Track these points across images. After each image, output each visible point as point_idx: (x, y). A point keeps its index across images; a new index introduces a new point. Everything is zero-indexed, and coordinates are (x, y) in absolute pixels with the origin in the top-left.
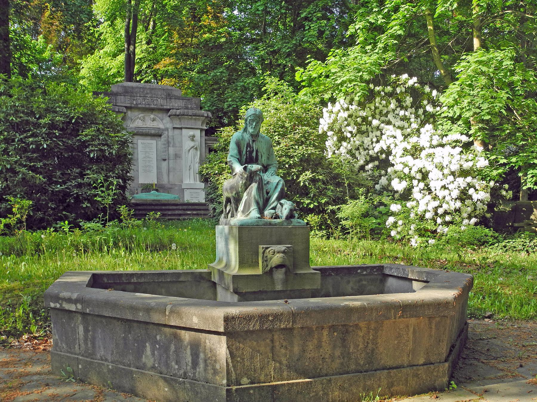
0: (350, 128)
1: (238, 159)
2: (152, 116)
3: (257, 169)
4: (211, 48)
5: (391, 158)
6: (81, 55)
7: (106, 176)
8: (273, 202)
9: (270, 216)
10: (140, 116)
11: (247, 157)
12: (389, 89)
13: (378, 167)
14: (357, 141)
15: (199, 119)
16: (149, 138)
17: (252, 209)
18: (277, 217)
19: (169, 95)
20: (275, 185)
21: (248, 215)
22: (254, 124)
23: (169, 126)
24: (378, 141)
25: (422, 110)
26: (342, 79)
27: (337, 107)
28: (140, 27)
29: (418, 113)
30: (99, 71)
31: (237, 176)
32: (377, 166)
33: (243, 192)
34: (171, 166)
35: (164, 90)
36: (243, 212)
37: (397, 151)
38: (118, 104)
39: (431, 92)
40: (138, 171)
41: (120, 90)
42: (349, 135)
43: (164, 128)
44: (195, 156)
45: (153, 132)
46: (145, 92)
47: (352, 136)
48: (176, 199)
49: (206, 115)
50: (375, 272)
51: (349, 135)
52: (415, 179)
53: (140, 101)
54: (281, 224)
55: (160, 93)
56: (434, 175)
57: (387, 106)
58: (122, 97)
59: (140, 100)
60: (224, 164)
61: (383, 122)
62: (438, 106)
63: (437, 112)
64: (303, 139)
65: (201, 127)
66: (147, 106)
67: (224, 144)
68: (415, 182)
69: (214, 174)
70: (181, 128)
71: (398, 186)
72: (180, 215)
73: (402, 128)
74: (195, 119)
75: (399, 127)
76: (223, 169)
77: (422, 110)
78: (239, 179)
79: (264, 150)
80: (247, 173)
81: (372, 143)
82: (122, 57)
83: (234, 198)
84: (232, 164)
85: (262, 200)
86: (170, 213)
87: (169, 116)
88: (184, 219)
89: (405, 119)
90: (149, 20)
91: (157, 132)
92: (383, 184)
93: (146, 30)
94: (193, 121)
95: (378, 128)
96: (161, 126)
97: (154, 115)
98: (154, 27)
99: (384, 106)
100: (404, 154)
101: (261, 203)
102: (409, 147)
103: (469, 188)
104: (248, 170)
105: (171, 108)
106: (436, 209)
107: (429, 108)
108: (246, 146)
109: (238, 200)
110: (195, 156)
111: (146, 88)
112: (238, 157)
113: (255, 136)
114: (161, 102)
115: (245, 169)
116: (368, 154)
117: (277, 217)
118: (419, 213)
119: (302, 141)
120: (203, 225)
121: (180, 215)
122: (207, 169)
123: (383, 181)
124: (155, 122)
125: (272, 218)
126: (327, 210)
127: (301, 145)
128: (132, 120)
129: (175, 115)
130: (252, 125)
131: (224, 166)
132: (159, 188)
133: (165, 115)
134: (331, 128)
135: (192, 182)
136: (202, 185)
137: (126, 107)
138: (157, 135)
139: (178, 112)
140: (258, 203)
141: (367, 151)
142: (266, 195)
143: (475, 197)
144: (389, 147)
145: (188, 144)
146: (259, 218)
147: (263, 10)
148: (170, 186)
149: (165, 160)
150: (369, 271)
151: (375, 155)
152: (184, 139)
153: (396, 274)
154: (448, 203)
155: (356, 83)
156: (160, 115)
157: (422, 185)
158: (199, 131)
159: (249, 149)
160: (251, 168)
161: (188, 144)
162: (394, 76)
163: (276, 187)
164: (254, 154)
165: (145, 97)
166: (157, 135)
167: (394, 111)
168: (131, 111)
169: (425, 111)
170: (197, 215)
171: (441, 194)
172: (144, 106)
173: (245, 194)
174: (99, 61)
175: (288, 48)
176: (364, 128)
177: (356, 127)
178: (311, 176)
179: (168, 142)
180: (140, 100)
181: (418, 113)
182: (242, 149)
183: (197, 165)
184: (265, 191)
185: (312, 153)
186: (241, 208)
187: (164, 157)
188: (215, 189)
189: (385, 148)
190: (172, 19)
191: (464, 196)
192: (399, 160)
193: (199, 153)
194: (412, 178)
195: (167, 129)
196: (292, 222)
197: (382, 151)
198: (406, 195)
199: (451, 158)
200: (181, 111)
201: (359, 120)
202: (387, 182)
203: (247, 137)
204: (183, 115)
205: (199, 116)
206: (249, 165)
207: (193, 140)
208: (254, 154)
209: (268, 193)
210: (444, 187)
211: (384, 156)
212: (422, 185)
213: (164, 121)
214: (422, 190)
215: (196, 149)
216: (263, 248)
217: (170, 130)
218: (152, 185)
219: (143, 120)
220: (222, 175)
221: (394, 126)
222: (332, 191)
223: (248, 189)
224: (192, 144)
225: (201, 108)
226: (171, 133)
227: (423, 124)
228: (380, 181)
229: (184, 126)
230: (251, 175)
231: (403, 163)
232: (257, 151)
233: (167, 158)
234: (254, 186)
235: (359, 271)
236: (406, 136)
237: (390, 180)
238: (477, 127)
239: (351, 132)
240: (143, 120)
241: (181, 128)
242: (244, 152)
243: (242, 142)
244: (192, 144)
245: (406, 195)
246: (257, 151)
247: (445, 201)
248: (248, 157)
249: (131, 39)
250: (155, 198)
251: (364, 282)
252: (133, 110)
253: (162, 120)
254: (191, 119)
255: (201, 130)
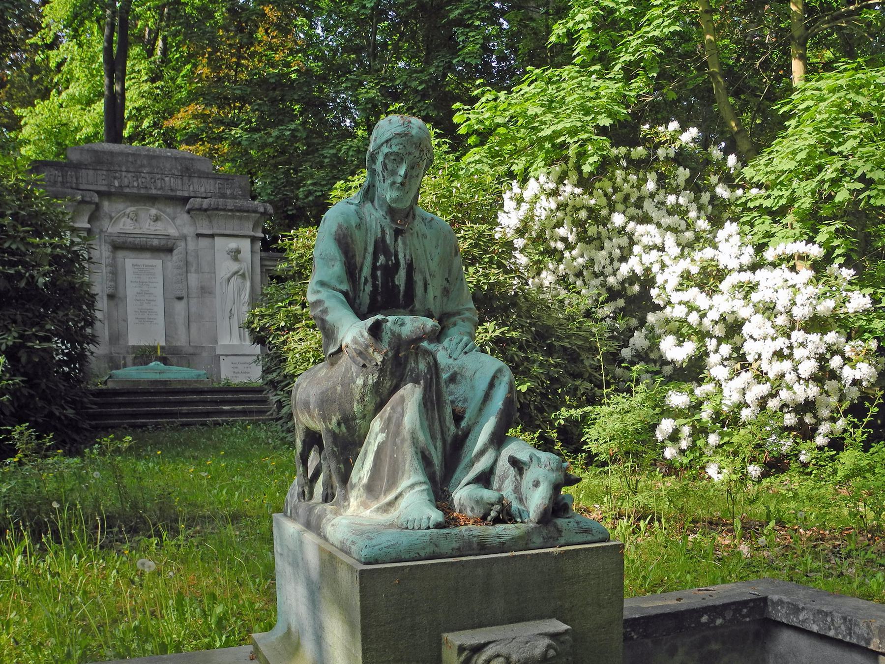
0: (562, 232)
1: (345, 294)
2: (153, 211)
3: (419, 333)
4: (273, 92)
5: (654, 292)
6: (28, 103)
7: (21, 336)
8: (482, 453)
9: (479, 512)
10: (128, 211)
11: (375, 286)
12: (639, 152)
13: (622, 312)
14: (577, 257)
15: (247, 218)
16: (148, 255)
17: (404, 483)
18: (506, 515)
19: (187, 169)
20: (482, 386)
21: (391, 504)
22: (402, 172)
23: (189, 230)
24: (624, 259)
25: (708, 194)
26: (553, 128)
27: (532, 187)
28: (135, 50)
29: (701, 202)
30: (59, 134)
31: (345, 360)
32: (622, 309)
33: (368, 417)
34: (193, 309)
35: (176, 159)
36: (371, 489)
37: (669, 278)
38: (81, 187)
39: (725, 159)
40: (126, 321)
41: (86, 158)
42: (560, 246)
43: (177, 234)
44: (240, 291)
45: (155, 242)
46: (139, 162)
47: (566, 248)
48: (201, 378)
49: (262, 210)
50: (744, 616)
51: (560, 246)
52: (711, 337)
53: (127, 180)
54: (523, 541)
55: (168, 166)
56: (755, 325)
57: (639, 187)
58: (91, 172)
59: (127, 178)
60: (298, 307)
61: (632, 218)
62: (738, 186)
63: (737, 199)
64: (476, 252)
65: (252, 234)
66: (143, 191)
67: (297, 264)
68: (711, 344)
69: (278, 329)
70: (212, 236)
71: (675, 351)
72: (208, 414)
73: (675, 230)
74: (240, 218)
75: (669, 228)
76: (297, 319)
77: (708, 194)
78: (354, 368)
79: (434, 265)
80: (385, 347)
81: (612, 261)
82: (100, 106)
83: (334, 436)
84: (325, 311)
85: (439, 443)
86: (185, 409)
87: (188, 212)
88: (217, 424)
89: (676, 210)
90: (156, 39)
91: (163, 242)
92: (638, 347)
93: (150, 56)
94: (236, 222)
95: (621, 231)
96: (172, 231)
97: (158, 209)
98: (165, 52)
99: (632, 187)
100: (682, 285)
101: (437, 458)
102: (695, 270)
103: (832, 355)
104: (386, 337)
105: (192, 194)
106: (762, 403)
107: (722, 191)
108: (371, 249)
109: (347, 446)
110: (240, 291)
111: (140, 155)
112: (345, 287)
113: (402, 216)
114: (172, 184)
115: (375, 331)
116: (604, 285)
117: (506, 515)
118: (726, 409)
119: (474, 257)
120: (256, 439)
121: (208, 414)
122: (262, 316)
123: (639, 339)
124: (159, 223)
125: (484, 518)
126: (556, 419)
127: (473, 264)
128: (111, 218)
129: (200, 209)
130: (394, 173)
131: (299, 312)
132: (168, 355)
133: (179, 209)
134: (521, 232)
135: (236, 341)
136: (257, 349)
137: (100, 193)
138: (165, 249)
139: (206, 203)
140: (425, 459)
141: (602, 278)
142: (453, 428)
143: (848, 373)
144: (648, 270)
145: (226, 267)
146: (438, 526)
147: (372, 9)
148: (191, 351)
149: (180, 298)
150: (729, 615)
151: (617, 287)
152: (218, 256)
153: (815, 628)
154: (790, 388)
155: (585, 136)
156: (169, 210)
157: (726, 349)
158: (248, 241)
159: (382, 259)
160: (396, 329)
161: (226, 267)
162: (647, 126)
163: (487, 397)
164: (401, 279)
165: (137, 174)
166: (165, 249)
167: (652, 196)
168: (110, 200)
169: (714, 197)
170: (244, 413)
171: (774, 369)
172: (135, 191)
173: (376, 424)
174: (59, 112)
175: (421, 83)
176: (592, 230)
177: (574, 229)
178: (497, 333)
179: (187, 264)
180: (127, 178)
181: (701, 202)
182: (358, 259)
183: (245, 308)
184: (448, 410)
185: (498, 283)
186: (362, 472)
187: (179, 293)
188: (281, 361)
189: (639, 270)
190: (194, 30)
191: (824, 375)
192: (675, 299)
193: (248, 284)
194: (702, 335)
195: (184, 238)
196: (559, 531)
197: (633, 278)
198: (693, 371)
199: (790, 289)
200: (213, 201)
201: (583, 214)
202: (646, 343)
203: (375, 215)
204: (217, 209)
205: (248, 211)
206: (391, 318)
207: (236, 259)
208: (401, 279)
209: (458, 418)
210: (779, 355)
211: (636, 288)
212: (726, 349)
213: (178, 222)
214: (726, 359)
215: (243, 276)
216: (461, 649)
217: (189, 239)
218: (154, 348)
219: (136, 219)
220: (294, 330)
221: (659, 225)
222: (541, 365)
223: (388, 408)
224: (235, 266)
225: (254, 198)
226: (191, 245)
227: (716, 222)
228: (632, 340)
229: (218, 232)
230: (396, 356)
231: (686, 304)
232: (410, 268)
233: (185, 295)
234: (410, 395)
235: (704, 619)
236: (686, 247)
237: (654, 339)
238: (833, 228)
239: (564, 240)
240: (136, 219)
241: (212, 236)
242: (366, 271)
243: (358, 235)
244: (235, 266)
245: (693, 371)
246: (410, 268)
247: (784, 385)
248: (379, 288)
249: (115, 66)
250: (158, 377)
251: (714, 646)
252: (113, 198)
253: (173, 219)
254: (232, 217)
255: (253, 239)
